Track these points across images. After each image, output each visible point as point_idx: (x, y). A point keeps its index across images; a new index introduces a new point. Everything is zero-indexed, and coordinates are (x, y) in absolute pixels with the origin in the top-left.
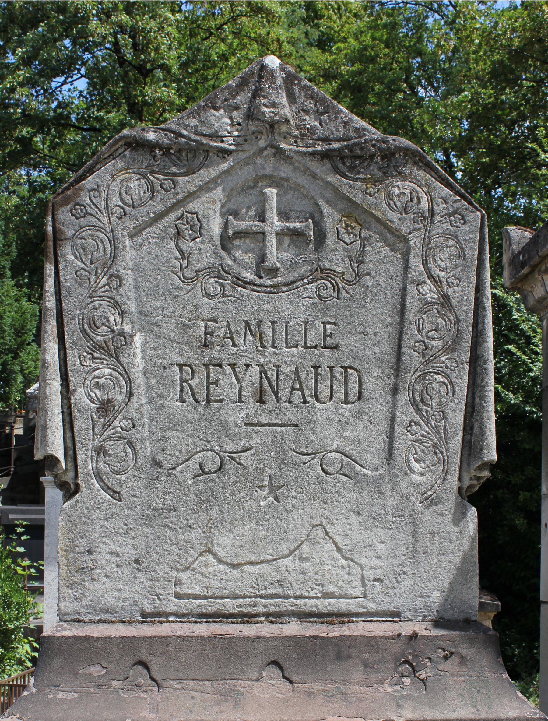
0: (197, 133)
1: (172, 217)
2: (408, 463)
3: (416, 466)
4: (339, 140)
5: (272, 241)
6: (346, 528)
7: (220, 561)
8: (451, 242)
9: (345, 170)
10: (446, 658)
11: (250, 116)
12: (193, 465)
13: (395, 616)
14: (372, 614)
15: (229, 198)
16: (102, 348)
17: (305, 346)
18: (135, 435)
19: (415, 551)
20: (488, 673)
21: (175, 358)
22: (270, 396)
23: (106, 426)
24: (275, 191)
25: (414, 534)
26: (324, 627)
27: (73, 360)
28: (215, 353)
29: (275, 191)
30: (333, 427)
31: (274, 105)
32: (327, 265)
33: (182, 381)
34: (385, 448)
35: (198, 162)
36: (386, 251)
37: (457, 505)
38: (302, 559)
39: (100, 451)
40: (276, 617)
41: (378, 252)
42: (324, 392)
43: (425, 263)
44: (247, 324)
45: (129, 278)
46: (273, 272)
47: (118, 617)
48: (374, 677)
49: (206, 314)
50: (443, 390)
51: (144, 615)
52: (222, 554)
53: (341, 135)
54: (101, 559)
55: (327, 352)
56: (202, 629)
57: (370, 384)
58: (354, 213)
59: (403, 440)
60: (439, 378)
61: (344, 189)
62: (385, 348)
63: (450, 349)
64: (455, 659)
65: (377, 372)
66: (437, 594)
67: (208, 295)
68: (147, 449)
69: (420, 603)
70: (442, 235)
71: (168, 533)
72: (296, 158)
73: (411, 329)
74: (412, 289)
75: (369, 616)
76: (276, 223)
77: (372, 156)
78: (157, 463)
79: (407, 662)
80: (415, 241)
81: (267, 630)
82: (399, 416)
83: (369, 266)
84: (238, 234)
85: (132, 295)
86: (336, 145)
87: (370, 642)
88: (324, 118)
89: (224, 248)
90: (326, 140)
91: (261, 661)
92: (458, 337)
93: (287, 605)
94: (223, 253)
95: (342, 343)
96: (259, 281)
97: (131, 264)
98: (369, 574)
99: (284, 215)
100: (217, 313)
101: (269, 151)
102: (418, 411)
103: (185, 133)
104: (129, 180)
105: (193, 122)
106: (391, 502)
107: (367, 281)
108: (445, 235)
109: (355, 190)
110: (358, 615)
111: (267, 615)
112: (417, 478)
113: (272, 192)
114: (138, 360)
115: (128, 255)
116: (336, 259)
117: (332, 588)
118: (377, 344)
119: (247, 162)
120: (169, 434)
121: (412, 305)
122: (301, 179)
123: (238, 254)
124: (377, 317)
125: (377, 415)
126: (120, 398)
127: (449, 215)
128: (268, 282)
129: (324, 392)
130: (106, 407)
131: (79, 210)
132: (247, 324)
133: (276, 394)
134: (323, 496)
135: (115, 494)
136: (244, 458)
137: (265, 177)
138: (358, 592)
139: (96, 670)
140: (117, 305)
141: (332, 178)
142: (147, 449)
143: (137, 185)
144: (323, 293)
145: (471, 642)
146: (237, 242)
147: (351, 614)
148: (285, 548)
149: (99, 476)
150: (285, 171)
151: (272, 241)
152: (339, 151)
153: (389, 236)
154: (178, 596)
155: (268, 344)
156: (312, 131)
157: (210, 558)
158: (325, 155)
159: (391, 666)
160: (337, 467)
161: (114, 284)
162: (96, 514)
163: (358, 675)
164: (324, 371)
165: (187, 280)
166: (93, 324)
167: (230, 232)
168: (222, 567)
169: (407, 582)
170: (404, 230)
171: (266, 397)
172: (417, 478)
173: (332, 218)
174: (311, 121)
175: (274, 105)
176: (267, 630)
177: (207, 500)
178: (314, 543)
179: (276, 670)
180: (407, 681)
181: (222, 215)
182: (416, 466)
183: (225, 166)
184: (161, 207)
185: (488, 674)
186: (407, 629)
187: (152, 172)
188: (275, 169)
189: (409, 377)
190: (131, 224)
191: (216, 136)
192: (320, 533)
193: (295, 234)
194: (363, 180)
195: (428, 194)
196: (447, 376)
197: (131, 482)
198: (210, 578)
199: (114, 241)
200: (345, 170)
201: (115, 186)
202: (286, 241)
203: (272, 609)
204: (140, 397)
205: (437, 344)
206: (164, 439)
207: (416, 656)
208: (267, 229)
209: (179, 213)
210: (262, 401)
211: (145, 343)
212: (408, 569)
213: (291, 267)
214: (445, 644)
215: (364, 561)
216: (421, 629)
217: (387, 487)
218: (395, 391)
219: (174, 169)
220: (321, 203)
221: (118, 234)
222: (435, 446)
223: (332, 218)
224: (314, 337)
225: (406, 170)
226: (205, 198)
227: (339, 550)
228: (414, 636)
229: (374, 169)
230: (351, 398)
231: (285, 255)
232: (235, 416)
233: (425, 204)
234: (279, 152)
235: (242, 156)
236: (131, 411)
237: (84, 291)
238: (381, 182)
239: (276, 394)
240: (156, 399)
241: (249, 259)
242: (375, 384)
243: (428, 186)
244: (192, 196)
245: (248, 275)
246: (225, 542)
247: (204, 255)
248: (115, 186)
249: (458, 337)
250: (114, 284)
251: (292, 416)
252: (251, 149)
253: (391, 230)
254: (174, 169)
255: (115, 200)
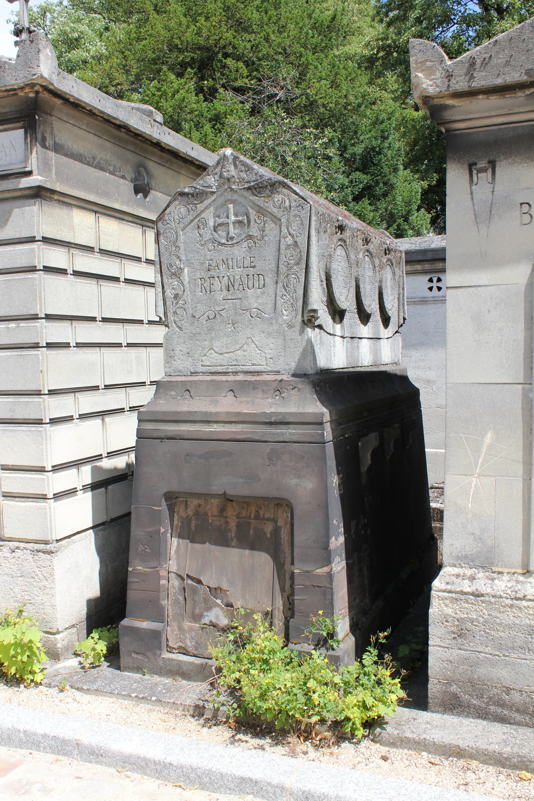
0: (203, 186)
1: (196, 221)
2: (282, 311)
3: (285, 313)
4: (253, 181)
5: (231, 226)
6: (260, 338)
7: (216, 352)
8: (298, 219)
9: (256, 193)
10: (293, 389)
11: (221, 176)
12: (205, 316)
13: (278, 372)
14: (270, 372)
15: (216, 210)
16: (174, 274)
17: (244, 267)
18: (186, 306)
19: (285, 346)
20: (308, 395)
21: (199, 276)
22: (231, 288)
23: (177, 303)
24: (232, 205)
25: (285, 340)
26: (251, 377)
27: (165, 280)
28: (212, 273)
29: (232, 205)
30: (255, 299)
31: (228, 171)
32: (251, 234)
33: (202, 284)
34: (273, 306)
35: (204, 198)
36: (273, 225)
37: (301, 328)
38: (244, 351)
39: (175, 313)
40: (235, 373)
41: (270, 226)
42: (251, 285)
43: (288, 229)
44: (223, 260)
45: (182, 246)
46: (232, 238)
47: (183, 374)
48: (265, 396)
49: (209, 258)
50: (295, 281)
51: (191, 373)
52: (216, 350)
53: (254, 179)
54: (177, 352)
55: (251, 269)
56: (209, 378)
57: (268, 280)
58: (261, 211)
59: (280, 301)
60: (293, 276)
61: (256, 202)
62: (273, 266)
63: (298, 264)
64: (296, 389)
65: (270, 275)
66: (293, 364)
67: (209, 250)
68: (190, 311)
69: (287, 367)
70: (294, 216)
71: (198, 342)
72: (238, 191)
73: (282, 257)
74: (282, 240)
75: (268, 373)
76: (233, 218)
77: (266, 186)
78: (194, 316)
79: (278, 390)
80: (283, 220)
81: (231, 378)
82: (278, 292)
83: (267, 232)
84: (220, 225)
85: (183, 253)
86: (252, 184)
87: (266, 382)
88: (248, 173)
89: (215, 231)
90: (249, 182)
91: (227, 389)
92: (300, 258)
93: (239, 368)
94: (214, 233)
95: (257, 265)
96: (227, 243)
97: (183, 241)
98: (268, 356)
99: (236, 215)
100: (213, 257)
101: (229, 190)
102: (286, 290)
103: (198, 187)
104: (180, 208)
105: (201, 182)
106: (275, 328)
107: (266, 238)
108: (295, 216)
109: (260, 201)
110: (265, 372)
111: (233, 372)
112: (285, 317)
113: (231, 206)
114: (186, 278)
115: (182, 238)
116: (254, 231)
117: (255, 362)
118: (270, 264)
119: (222, 195)
120: (197, 305)
121: (283, 247)
122: (241, 200)
123: (220, 232)
124: (269, 253)
125: (271, 293)
126: (181, 293)
127: (297, 207)
128: (230, 243)
129: (251, 285)
130: (176, 296)
131: (165, 223)
132: (223, 260)
133: (233, 287)
134: (251, 326)
135: (180, 328)
136: (223, 313)
137: (228, 200)
138: (264, 363)
139: (173, 393)
140: (179, 257)
141: (253, 198)
142: (190, 311)
143: (183, 210)
144: (250, 245)
145: (303, 382)
146: (219, 228)
147: (262, 372)
148: (238, 347)
149: (175, 322)
150: (235, 197)
151: (231, 226)
152: (254, 186)
153: (274, 219)
154: (202, 366)
155: (230, 268)
156: (243, 179)
157: (213, 351)
158: (249, 188)
159: (272, 392)
160: (256, 314)
161: (177, 250)
162: (174, 336)
163: (260, 395)
164: (251, 277)
165: (202, 245)
166: (171, 266)
167: (216, 225)
168: (216, 355)
169: (282, 359)
170: (279, 216)
171: (230, 289)
172: (285, 317)
173: (252, 213)
174: (243, 175)
175: (228, 171)
176: (231, 378)
177: (211, 329)
178: (248, 345)
179: (232, 393)
180: (277, 397)
181: (214, 217)
182: (285, 313)
183: (213, 198)
184: (192, 218)
185: (308, 395)
186: (279, 378)
187: (188, 204)
188: (232, 196)
189: (282, 277)
190: (182, 225)
191: (209, 187)
192: (250, 340)
193: (240, 222)
194: (264, 197)
195: (289, 199)
196: (296, 275)
197: (185, 324)
198: (214, 359)
199: (176, 233)
200: (256, 193)
201: (176, 212)
202: (237, 225)
203: (234, 370)
204: (187, 292)
205: (292, 262)
206: (196, 307)
207: (282, 388)
208: (229, 222)
209: (198, 219)
210: (229, 290)
211: (189, 271)
212: (282, 354)
213: (239, 235)
214: (293, 383)
215: (266, 351)
216: (285, 377)
217: (274, 321)
218: (277, 282)
219: (196, 202)
220: (249, 208)
221: (178, 230)
222: (292, 304)
223: (252, 213)
224: (247, 263)
225: (280, 190)
226: (207, 212)
227: (257, 347)
228: (281, 380)
229: (267, 192)
230: (261, 287)
231: (237, 231)
232: (219, 296)
233: (287, 204)
234: (232, 190)
235: (219, 193)
236: (184, 298)
237: (167, 253)
238: (270, 196)
239: (233, 287)
240: (193, 292)
241: (224, 234)
242: (269, 280)
243: (288, 195)
244: (202, 212)
245: (223, 241)
246: (217, 345)
247: (208, 234)
248: (176, 212)
249: (300, 258)
250: (177, 250)
251: (239, 295)
252: (222, 190)
253: (275, 217)
254: (196, 202)
255: (177, 217)
